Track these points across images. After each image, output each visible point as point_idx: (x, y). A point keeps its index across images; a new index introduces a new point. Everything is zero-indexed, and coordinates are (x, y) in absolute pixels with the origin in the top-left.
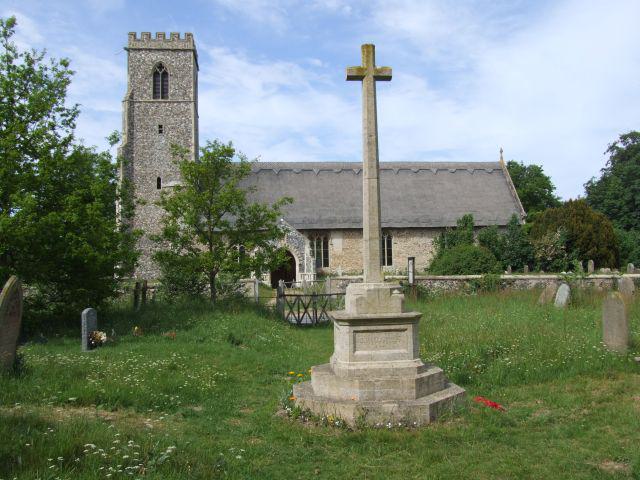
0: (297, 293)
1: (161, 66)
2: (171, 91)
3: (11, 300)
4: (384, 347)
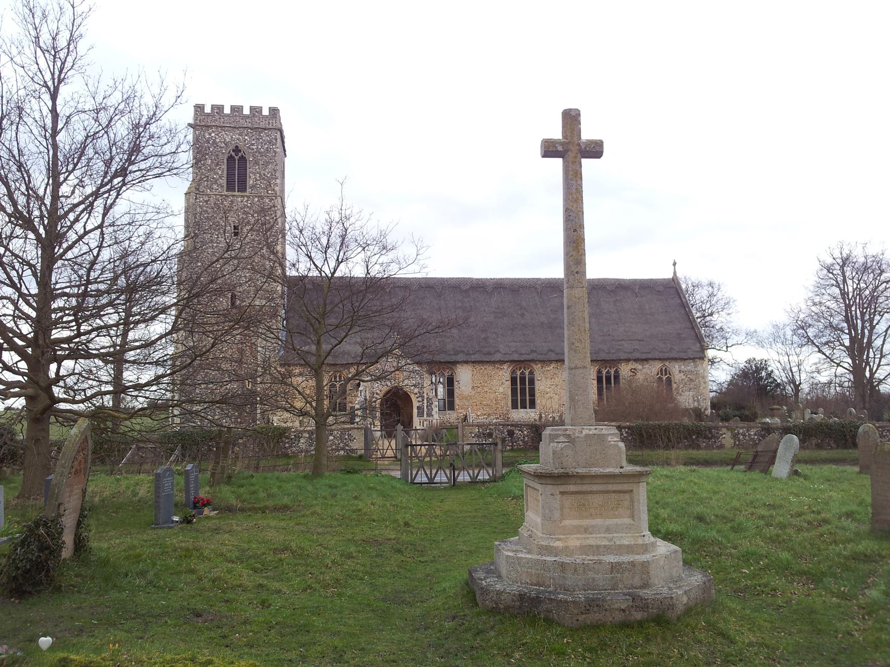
0: (15, 445)
1: (237, 150)
2: (250, 182)
3: (78, 452)
4: (601, 515)
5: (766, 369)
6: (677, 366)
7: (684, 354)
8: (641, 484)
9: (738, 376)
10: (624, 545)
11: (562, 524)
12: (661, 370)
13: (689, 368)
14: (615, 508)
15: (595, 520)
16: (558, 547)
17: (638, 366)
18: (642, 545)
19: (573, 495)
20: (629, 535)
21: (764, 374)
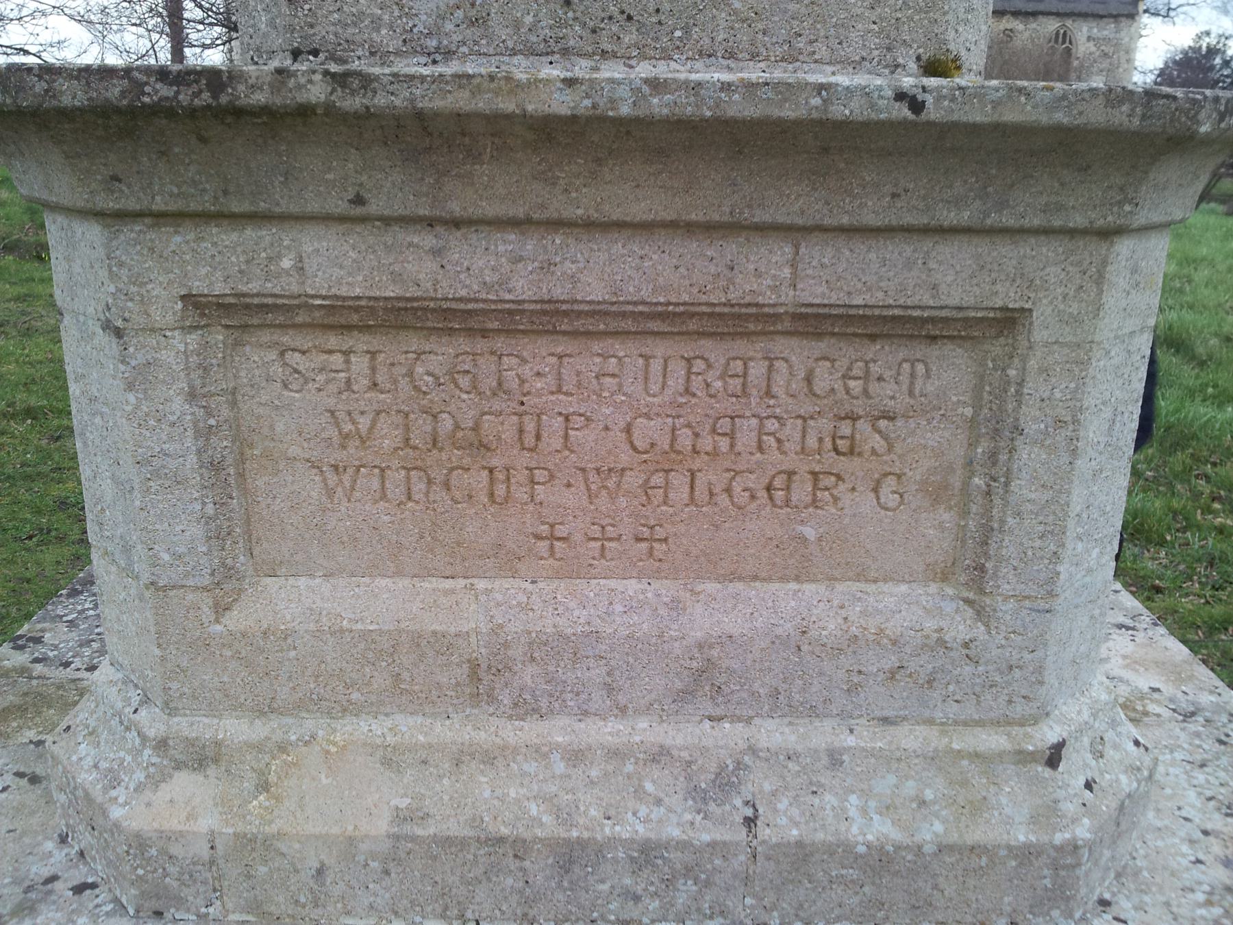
5: (1224, 52)
6: (1085, 29)
7: (1102, 6)
8: (1124, 247)
9: (1175, 62)
10: (842, 851)
11: (235, 620)
12: (1057, 34)
13: (1106, 33)
14: (803, 490)
15: (591, 588)
16: (168, 837)
17: (1017, 25)
18: (1026, 854)
19: (361, 342)
20: (911, 738)
21: (1218, 61)
